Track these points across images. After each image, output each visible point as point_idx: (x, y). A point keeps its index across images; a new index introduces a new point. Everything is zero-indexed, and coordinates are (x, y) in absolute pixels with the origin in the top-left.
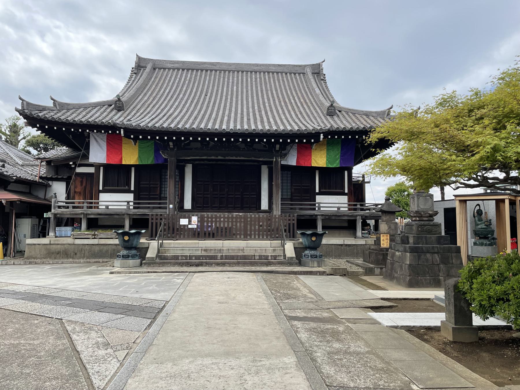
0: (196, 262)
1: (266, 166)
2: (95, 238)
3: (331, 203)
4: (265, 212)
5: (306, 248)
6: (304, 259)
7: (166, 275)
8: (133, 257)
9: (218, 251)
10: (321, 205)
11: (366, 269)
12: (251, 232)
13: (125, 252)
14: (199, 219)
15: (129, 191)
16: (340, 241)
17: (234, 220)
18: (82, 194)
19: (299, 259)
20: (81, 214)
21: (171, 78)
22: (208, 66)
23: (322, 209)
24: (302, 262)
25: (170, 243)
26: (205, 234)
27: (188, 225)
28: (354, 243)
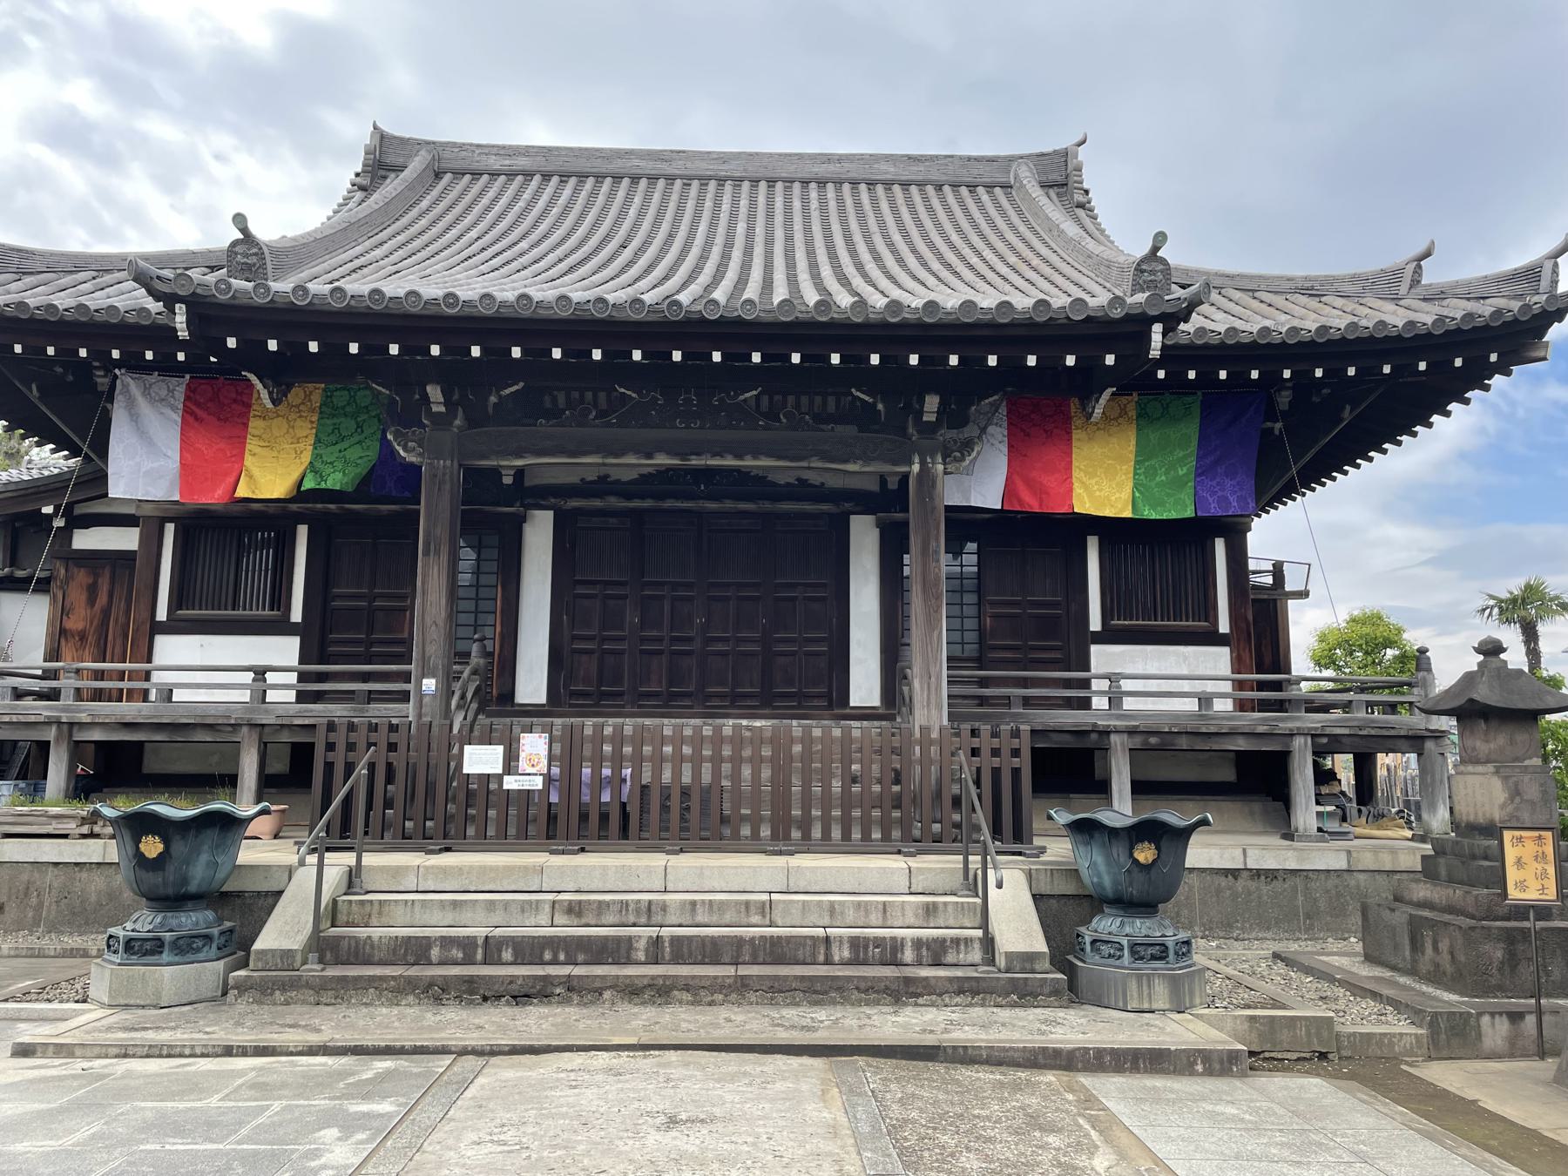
0: (512, 979)
1: (869, 520)
2: (92, 835)
3: (1160, 682)
4: (865, 714)
5: (1095, 902)
6: (1090, 965)
8: (186, 948)
9: (638, 912)
10: (1127, 685)
11: (1434, 1022)
12: (806, 808)
13: (143, 922)
14: (557, 748)
16: (1228, 853)
17: (727, 751)
18: (91, 639)
19: (1067, 973)
20: (48, 723)
21: (495, 200)
22: (642, 164)
23: (1129, 704)
24: (1083, 980)
25: (398, 871)
26: (584, 817)
27: (500, 778)
28: (1292, 865)
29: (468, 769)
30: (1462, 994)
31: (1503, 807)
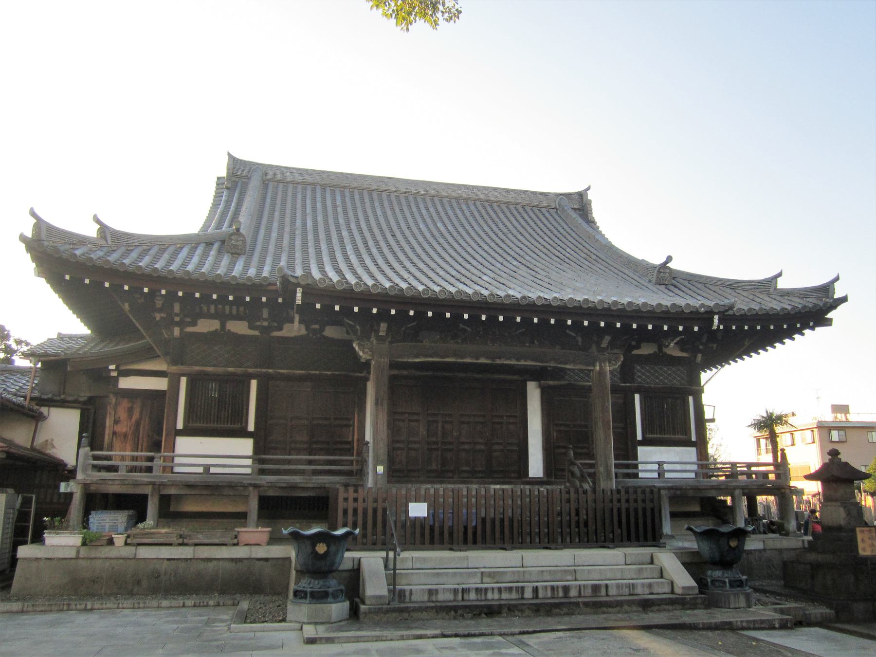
7: (464, 646)
10: (666, 467)
15: (242, 433)
29: (425, 505)
30: (796, 601)
31: (844, 519)
